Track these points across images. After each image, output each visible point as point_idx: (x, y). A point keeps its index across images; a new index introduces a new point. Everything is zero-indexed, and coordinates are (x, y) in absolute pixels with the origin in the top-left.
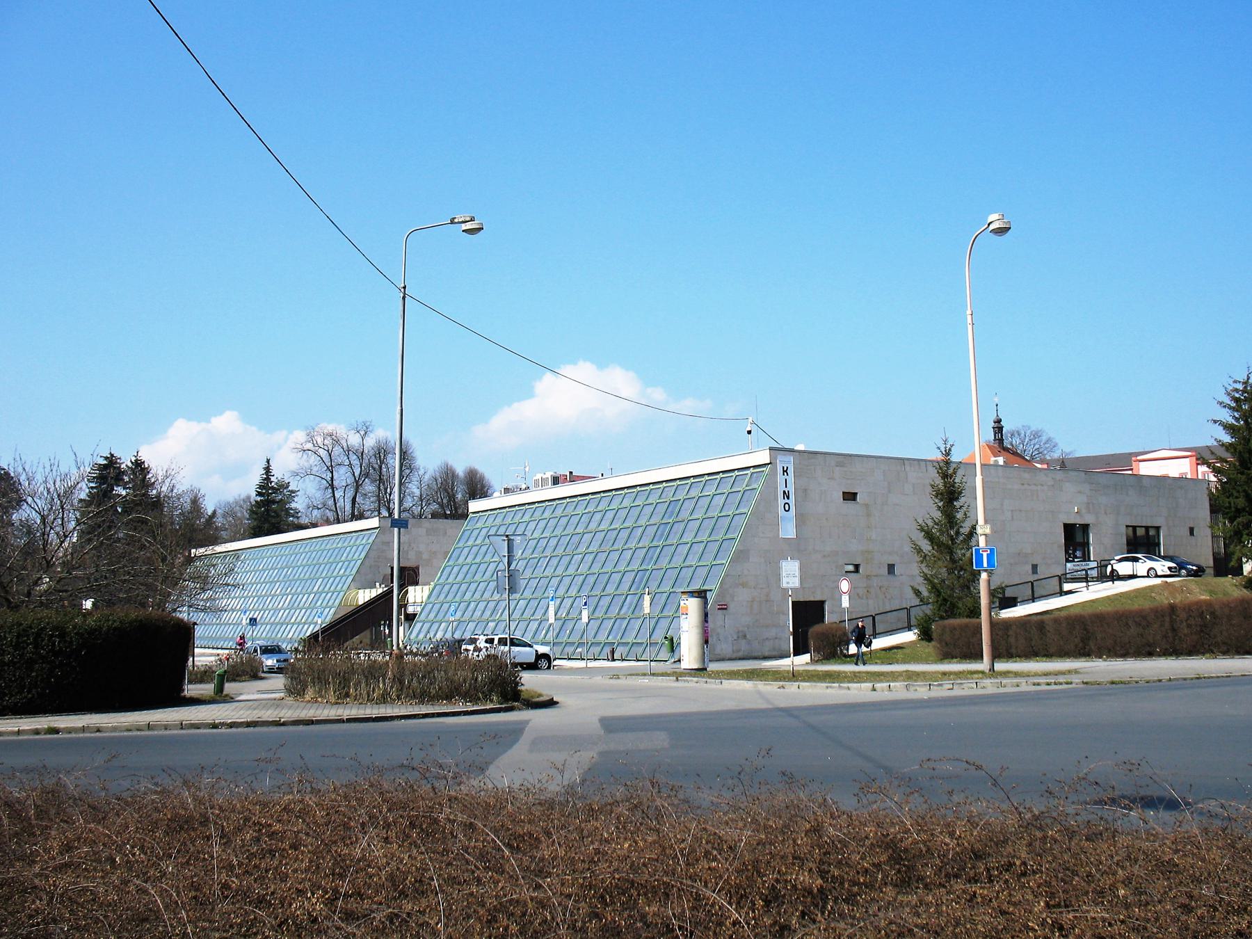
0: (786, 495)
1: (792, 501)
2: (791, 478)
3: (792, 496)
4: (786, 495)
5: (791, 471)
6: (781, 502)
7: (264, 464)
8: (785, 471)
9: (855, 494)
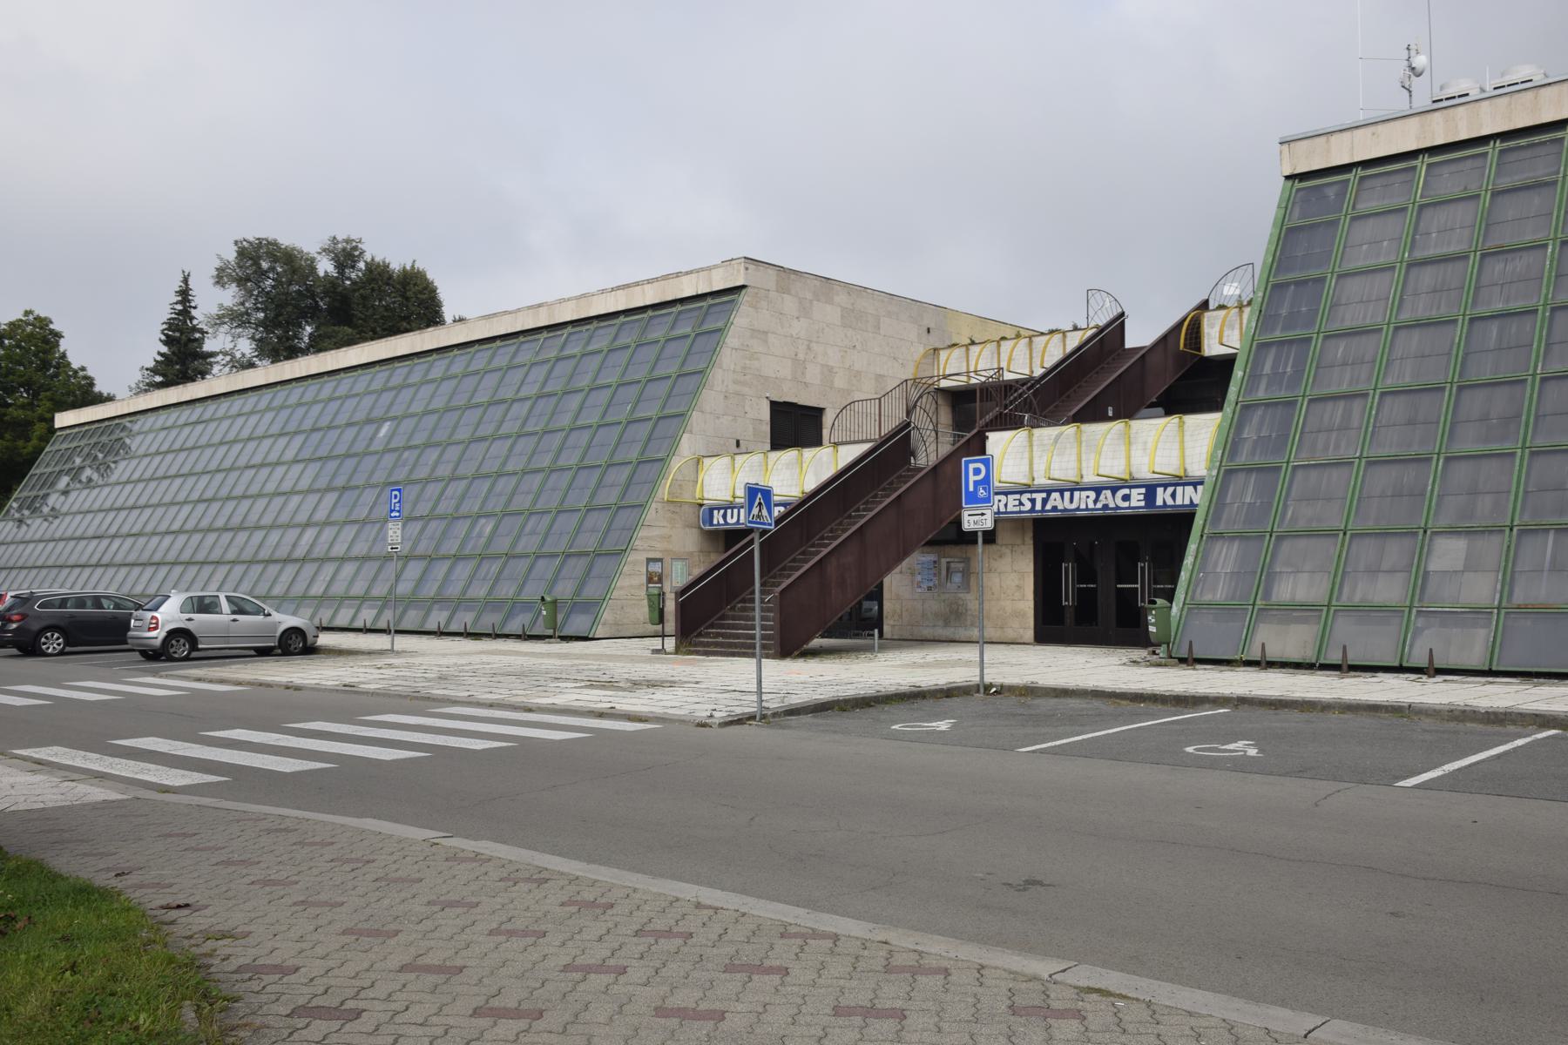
7: (177, 284)
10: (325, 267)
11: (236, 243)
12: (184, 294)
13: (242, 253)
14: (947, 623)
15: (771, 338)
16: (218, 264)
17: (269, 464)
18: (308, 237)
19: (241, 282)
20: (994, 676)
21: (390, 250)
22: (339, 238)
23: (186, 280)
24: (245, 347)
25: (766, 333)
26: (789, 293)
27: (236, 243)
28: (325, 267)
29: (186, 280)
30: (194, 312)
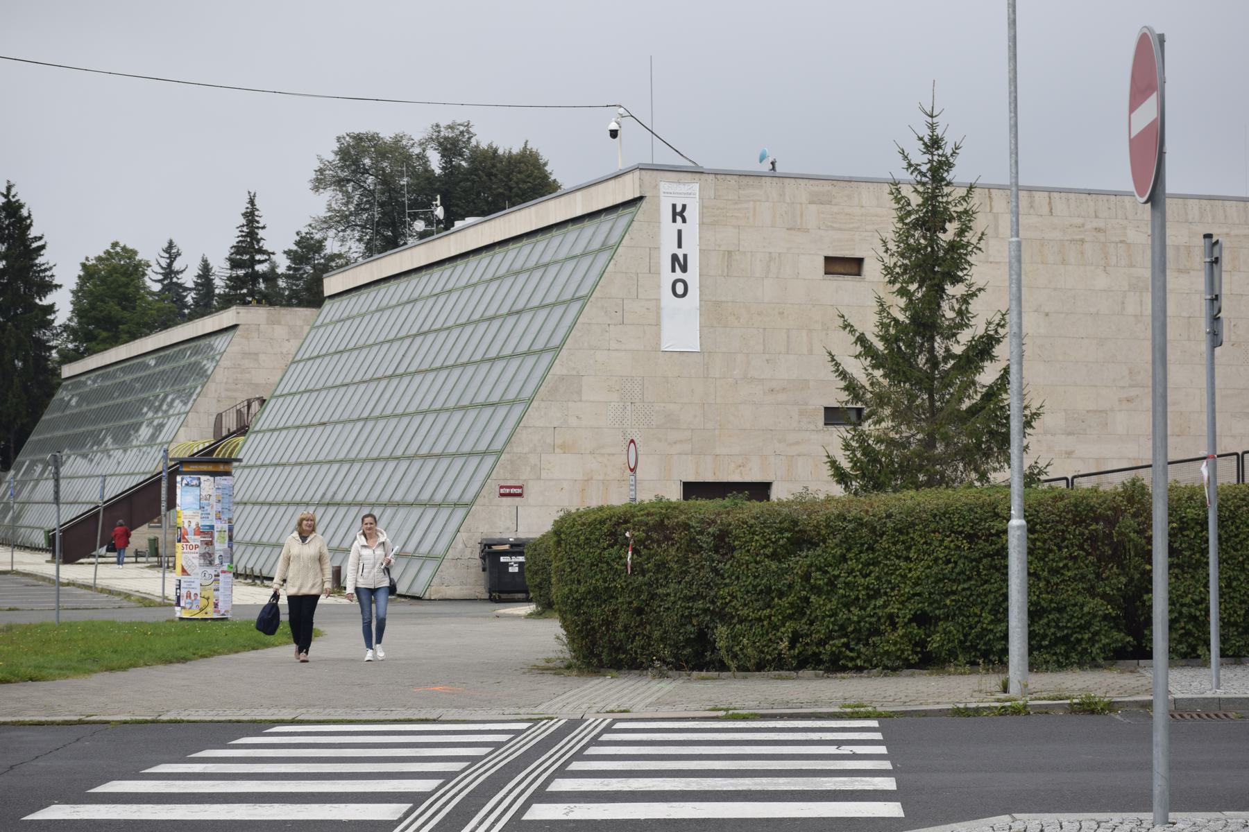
0: (679, 263)
1: (692, 276)
2: (691, 230)
3: (693, 264)
4: (679, 263)
5: (692, 214)
6: (667, 277)
7: (243, 206)
8: (678, 214)
9: (859, 262)
10: (435, 162)
11: (338, 139)
12: (251, 216)
13: (344, 153)
14: (70, 557)
15: (262, 357)
16: (317, 165)
17: (535, 353)
18: (410, 123)
19: (340, 183)
20: (101, 583)
21: (498, 134)
22: (443, 124)
23: (252, 202)
24: (355, 248)
25: (256, 354)
26: (279, 323)
27: (338, 139)
28: (435, 162)
29: (252, 202)
30: (261, 233)
